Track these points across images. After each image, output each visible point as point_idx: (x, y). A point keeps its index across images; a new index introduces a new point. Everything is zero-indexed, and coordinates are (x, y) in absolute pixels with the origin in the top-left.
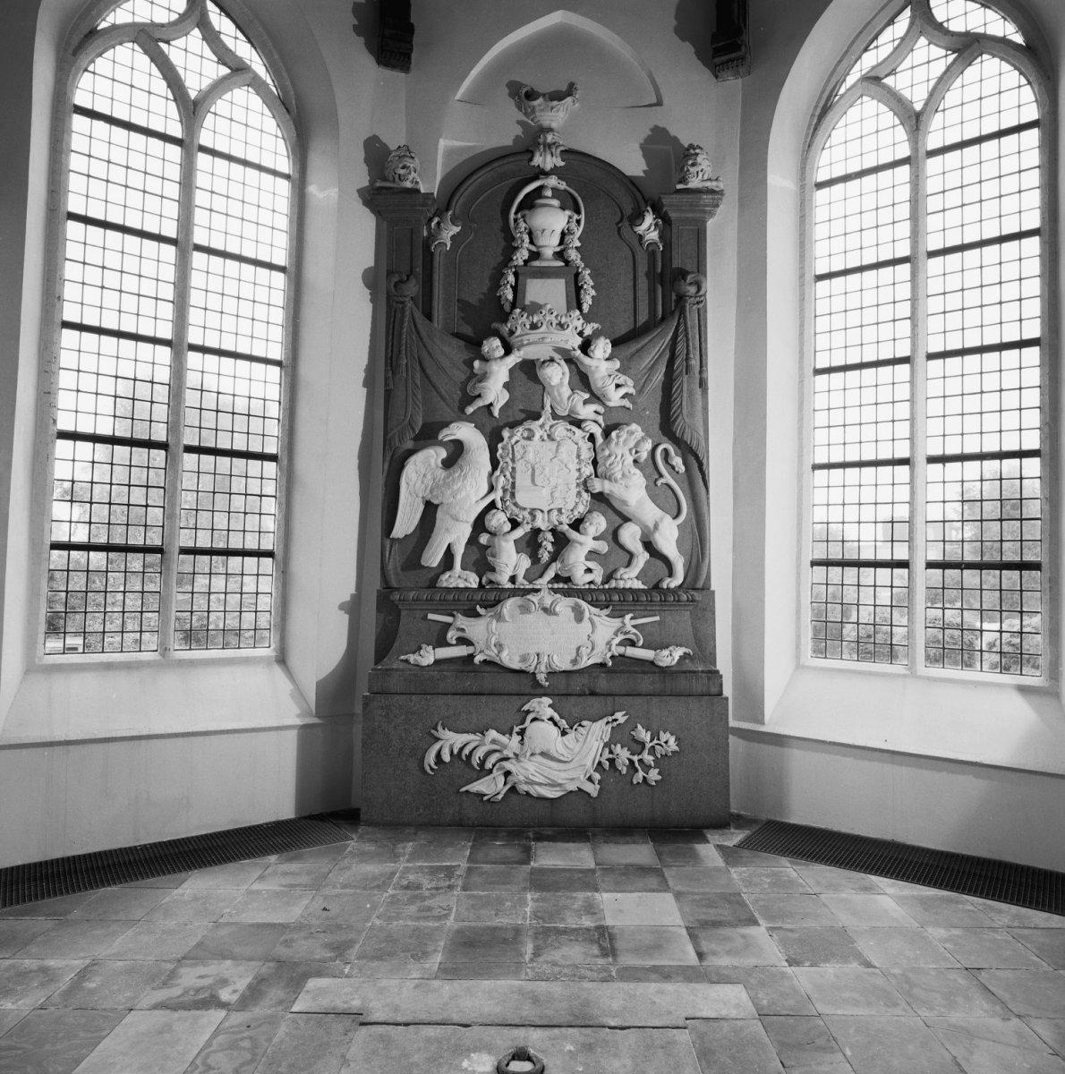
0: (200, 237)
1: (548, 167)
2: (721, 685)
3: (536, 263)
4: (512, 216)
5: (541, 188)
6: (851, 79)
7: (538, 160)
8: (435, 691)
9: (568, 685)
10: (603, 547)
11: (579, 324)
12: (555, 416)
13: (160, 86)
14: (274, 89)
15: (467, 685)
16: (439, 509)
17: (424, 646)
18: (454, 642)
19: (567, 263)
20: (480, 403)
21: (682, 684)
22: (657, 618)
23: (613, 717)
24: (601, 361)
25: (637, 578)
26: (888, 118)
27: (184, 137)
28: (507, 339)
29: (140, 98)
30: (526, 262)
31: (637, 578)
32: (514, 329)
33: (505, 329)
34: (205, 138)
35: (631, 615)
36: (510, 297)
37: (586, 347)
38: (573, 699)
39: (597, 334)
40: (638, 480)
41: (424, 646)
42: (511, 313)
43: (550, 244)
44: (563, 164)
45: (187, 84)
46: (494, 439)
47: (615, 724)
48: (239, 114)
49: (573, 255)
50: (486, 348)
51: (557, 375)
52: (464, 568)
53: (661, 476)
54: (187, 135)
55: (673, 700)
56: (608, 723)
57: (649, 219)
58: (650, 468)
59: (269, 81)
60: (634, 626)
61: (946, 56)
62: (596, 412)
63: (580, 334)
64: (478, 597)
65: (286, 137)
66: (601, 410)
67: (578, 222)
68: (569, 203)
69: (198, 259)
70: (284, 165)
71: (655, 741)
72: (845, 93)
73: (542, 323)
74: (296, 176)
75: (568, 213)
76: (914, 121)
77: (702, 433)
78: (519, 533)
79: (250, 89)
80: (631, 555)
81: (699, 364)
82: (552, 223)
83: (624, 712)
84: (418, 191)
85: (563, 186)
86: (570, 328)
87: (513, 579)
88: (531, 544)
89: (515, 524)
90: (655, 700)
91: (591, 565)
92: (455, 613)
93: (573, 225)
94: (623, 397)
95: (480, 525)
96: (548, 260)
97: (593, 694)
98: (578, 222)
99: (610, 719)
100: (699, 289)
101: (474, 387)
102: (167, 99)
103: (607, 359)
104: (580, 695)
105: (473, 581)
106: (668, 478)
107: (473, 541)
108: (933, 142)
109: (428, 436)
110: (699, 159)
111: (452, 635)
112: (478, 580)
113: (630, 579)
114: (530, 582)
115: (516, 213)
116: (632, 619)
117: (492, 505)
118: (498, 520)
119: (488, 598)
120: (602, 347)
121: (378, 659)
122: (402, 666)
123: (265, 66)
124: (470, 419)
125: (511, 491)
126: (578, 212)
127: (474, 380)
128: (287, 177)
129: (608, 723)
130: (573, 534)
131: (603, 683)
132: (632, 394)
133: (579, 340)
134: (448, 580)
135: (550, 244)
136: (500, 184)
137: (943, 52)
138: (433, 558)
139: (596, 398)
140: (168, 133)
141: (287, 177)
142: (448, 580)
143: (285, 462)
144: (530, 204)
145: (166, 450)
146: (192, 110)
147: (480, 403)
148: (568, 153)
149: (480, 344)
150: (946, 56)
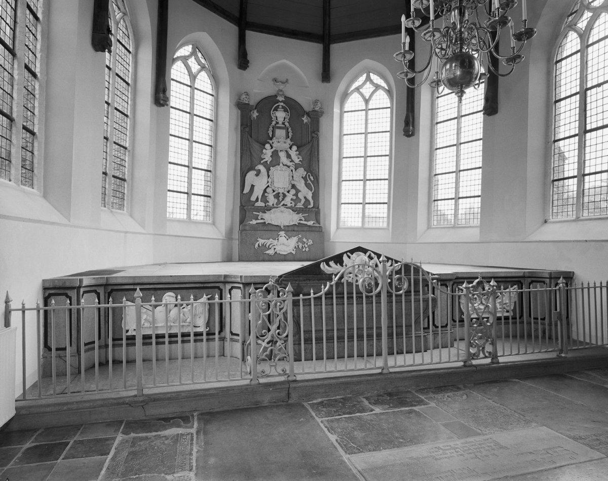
1: (281, 100)
12: (284, 165)
13: (186, 72)
19: (285, 125)
20: (264, 160)
21: (314, 229)
24: (293, 152)
26: (361, 99)
33: (271, 142)
37: (291, 148)
38: (289, 232)
39: (293, 145)
43: (281, 120)
46: (268, 170)
49: (287, 124)
50: (266, 147)
51: (282, 155)
52: (261, 201)
57: (305, 116)
58: (305, 178)
63: (290, 144)
68: (285, 110)
76: (367, 101)
78: (275, 193)
80: (301, 200)
82: (281, 115)
88: (277, 196)
91: (292, 202)
93: (287, 116)
95: (265, 191)
97: (294, 231)
105: (263, 205)
106: (309, 182)
109: (252, 168)
111: (259, 218)
113: (300, 205)
117: (268, 186)
118: (269, 190)
119: (266, 209)
120: (295, 148)
124: (262, 164)
125: (272, 182)
126: (288, 113)
130: (287, 194)
133: (289, 146)
134: (256, 204)
135: (281, 120)
136: (268, 103)
138: (253, 198)
139: (292, 161)
142: (256, 204)
144: (276, 109)
147: (264, 160)
148: (285, 97)
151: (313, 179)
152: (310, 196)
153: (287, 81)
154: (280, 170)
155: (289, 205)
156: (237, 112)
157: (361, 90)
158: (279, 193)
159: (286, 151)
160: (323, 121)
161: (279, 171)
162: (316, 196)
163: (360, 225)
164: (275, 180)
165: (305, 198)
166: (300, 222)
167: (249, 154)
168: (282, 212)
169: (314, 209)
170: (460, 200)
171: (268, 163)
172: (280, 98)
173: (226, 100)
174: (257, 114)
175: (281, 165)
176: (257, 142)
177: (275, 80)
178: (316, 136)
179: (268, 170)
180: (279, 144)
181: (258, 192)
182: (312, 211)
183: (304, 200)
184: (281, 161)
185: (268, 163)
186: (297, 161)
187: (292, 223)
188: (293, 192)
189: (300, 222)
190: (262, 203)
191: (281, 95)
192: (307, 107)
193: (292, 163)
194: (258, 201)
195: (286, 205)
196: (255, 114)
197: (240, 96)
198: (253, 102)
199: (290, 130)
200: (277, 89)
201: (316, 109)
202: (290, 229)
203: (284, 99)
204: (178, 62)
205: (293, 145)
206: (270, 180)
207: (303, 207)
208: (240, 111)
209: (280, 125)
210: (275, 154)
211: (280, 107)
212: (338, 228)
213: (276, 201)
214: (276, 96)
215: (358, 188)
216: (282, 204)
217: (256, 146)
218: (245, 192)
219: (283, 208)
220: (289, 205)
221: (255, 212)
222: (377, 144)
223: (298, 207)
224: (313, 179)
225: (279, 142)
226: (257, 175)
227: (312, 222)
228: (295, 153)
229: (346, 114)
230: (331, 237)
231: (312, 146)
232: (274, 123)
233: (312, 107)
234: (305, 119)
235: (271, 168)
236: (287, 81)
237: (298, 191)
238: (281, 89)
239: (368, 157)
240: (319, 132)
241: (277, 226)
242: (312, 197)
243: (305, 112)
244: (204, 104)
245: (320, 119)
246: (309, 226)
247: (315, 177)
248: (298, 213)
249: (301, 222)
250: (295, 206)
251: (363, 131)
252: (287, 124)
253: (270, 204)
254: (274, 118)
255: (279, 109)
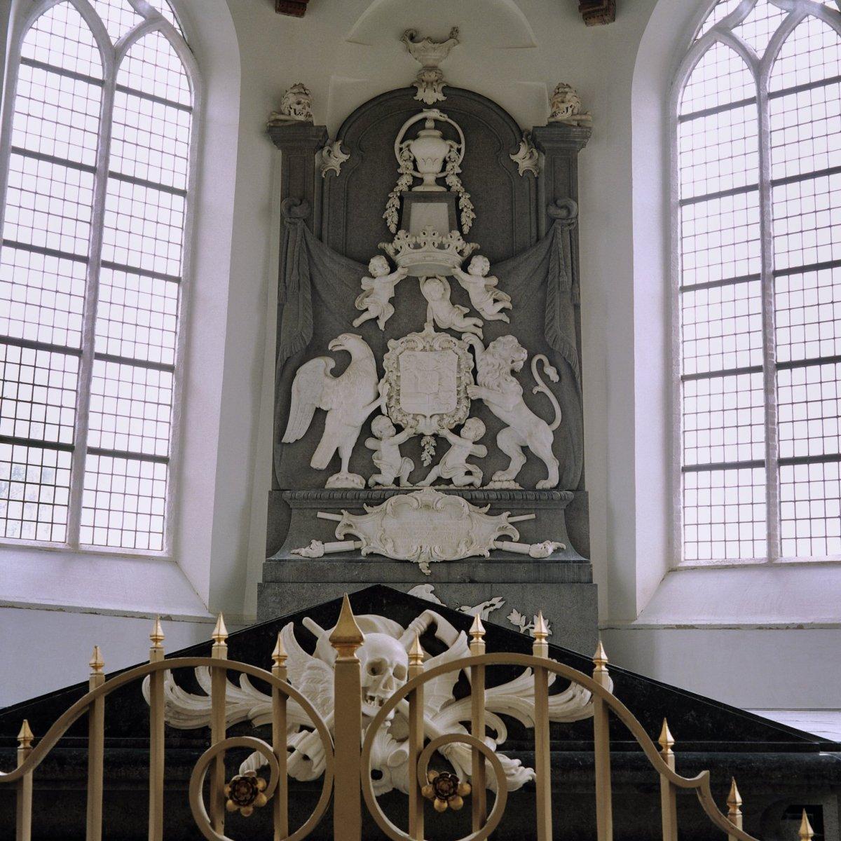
0: (114, 166)
1: (430, 102)
2: (591, 574)
3: (417, 189)
4: (397, 146)
5: (425, 119)
6: (707, 27)
7: (420, 95)
8: (326, 580)
9: (449, 574)
10: (482, 451)
11: (461, 244)
12: (437, 329)
13: (87, 36)
14: (180, 32)
15: (355, 574)
16: (329, 414)
17: (313, 541)
18: (343, 538)
19: (449, 188)
20: (365, 317)
21: (555, 572)
22: (533, 516)
23: (491, 602)
24: (477, 280)
25: (515, 480)
26: (739, 62)
27: (105, 79)
28: (393, 258)
29: (71, 47)
30: (410, 187)
31: (515, 480)
32: (446, 246)
33: (390, 249)
34: (121, 79)
35: (508, 513)
36: (396, 219)
37: (465, 266)
38: (454, 586)
39: (475, 253)
40: (514, 388)
41: (313, 541)
42: (397, 234)
43: (430, 170)
44: (444, 98)
45: (110, 33)
46: (379, 352)
47: (492, 609)
48: (150, 57)
49: (453, 181)
50: (371, 268)
51: (435, 294)
52: (350, 471)
53: (537, 385)
54: (108, 77)
55: (547, 587)
56: (485, 608)
57: (524, 149)
58: (523, 376)
59: (176, 26)
60: (512, 524)
61: (781, 14)
62: (475, 325)
63: (461, 253)
64: (362, 495)
65: (189, 74)
66: (480, 323)
67: (459, 150)
68: (447, 133)
69: (112, 184)
70: (186, 99)
71: (530, 625)
72: (701, 38)
73: (449, 245)
74: (198, 108)
75: (450, 142)
76: (760, 68)
77: (574, 345)
78: (402, 437)
79: (160, 34)
81: (571, 280)
82: (430, 153)
83: (500, 598)
84: (311, 123)
85: (444, 118)
86: (451, 247)
87: (397, 481)
88: (412, 448)
89: (399, 429)
90: (529, 586)
92: (343, 511)
93: (454, 154)
94: (501, 311)
95: (366, 430)
96: (427, 185)
97: (472, 581)
98: (459, 150)
99: (487, 603)
100: (569, 212)
101: (361, 301)
102: (92, 46)
103: (486, 276)
104: (460, 583)
105: (356, 482)
106: (542, 387)
107: (359, 445)
108: (773, 86)
109: (316, 348)
110: (569, 96)
111: (339, 532)
112: (364, 482)
113: (504, 480)
114: (414, 484)
115: (402, 142)
116: (509, 516)
117: (378, 412)
118: (379, 425)
119: (371, 498)
120: (480, 265)
121: (271, 550)
122: (293, 557)
123: (173, 12)
124: (358, 331)
125: (395, 395)
126: (459, 142)
127: (362, 295)
128: (189, 109)
129: (485, 608)
130: (452, 438)
131: (481, 573)
132: (509, 309)
133: (459, 259)
134: (334, 482)
135: (430, 170)
136: (388, 115)
137: (779, 11)
138: (321, 459)
139: (473, 313)
140: (125, 95)
141: (189, 109)
142: (334, 482)
143: (182, 371)
144: (412, 134)
145: (80, 357)
146: (113, 54)
147: (365, 317)
148: (447, 90)
149: (367, 263)
150: (781, 14)
151: (554, 377)
152: (542, 439)
153: (454, 33)
154: (424, 349)
155: (460, 480)
156: (267, 157)
157: (736, 32)
158: (422, 436)
159: (451, 280)
160: (593, 163)
161: (418, 354)
162: (569, 443)
163: (761, 553)
164: (405, 386)
165: (525, 449)
166: (500, 545)
167: (309, 297)
168: (427, 507)
169: (557, 494)
170: (779, 279)
171: (381, 325)
172: (430, 95)
173: (226, 111)
174: (344, 158)
175: (429, 328)
176: (345, 254)
177: (412, 37)
178: (563, 213)
179: (379, 352)
180: (418, 254)
181: (340, 435)
182: (558, 502)
183: (523, 460)
184: (429, 318)
185: (381, 325)
186: (491, 311)
187: (464, 552)
188: (475, 428)
189: (500, 545)
190: (351, 476)
191: (430, 84)
192: (529, 115)
193: (471, 321)
194: (339, 471)
195: (450, 481)
196: (337, 158)
197: (278, 100)
198: (329, 116)
199: (464, 201)
200: (419, 65)
201: (560, 117)
202: (458, 572)
203: (441, 97)
204: (148, 36)
205: (475, 253)
206: (384, 388)
207: (517, 486)
208: (280, 152)
209: (430, 186)
210: (408, 293)
211: (429, 124)
212: (672, 569)
213: (409, 466)
214: (413, 89)
215: (744, 400)
216: (432, 476)
217: (332, 267)
218: (289, 437)
219: (440, 499)
220: (460, 480)
221: (325, 510)
222: (809, 222)
223: (497, 486)
224: (554, 377)
225: (417, 246)
226: (337, 373)
227: (550, 547)
228: (483, 282)
229: (683, 129)
230: (640, 605)
231: (549, 251)
232: (404, 182)
233: (549, 112)
234: (523, 158)
235: (391, 343)
236: (454, 33)
237: (495, 425)
238: (431, 63)
239: (777, 273)
240: (576, 200)
241: (407, 561)
242: (554, 447)
243: (521, 132)
244: (158, 138)
245: (582, 154)
246: (538, 561)
247: (564, 369)
248: (493, 512)
249: (506, 546)
250: (482, 485)
251: (754, 179)
252: (453, 181)
253: (386, 478)
254: (405, 166)
255: (422, 133)
